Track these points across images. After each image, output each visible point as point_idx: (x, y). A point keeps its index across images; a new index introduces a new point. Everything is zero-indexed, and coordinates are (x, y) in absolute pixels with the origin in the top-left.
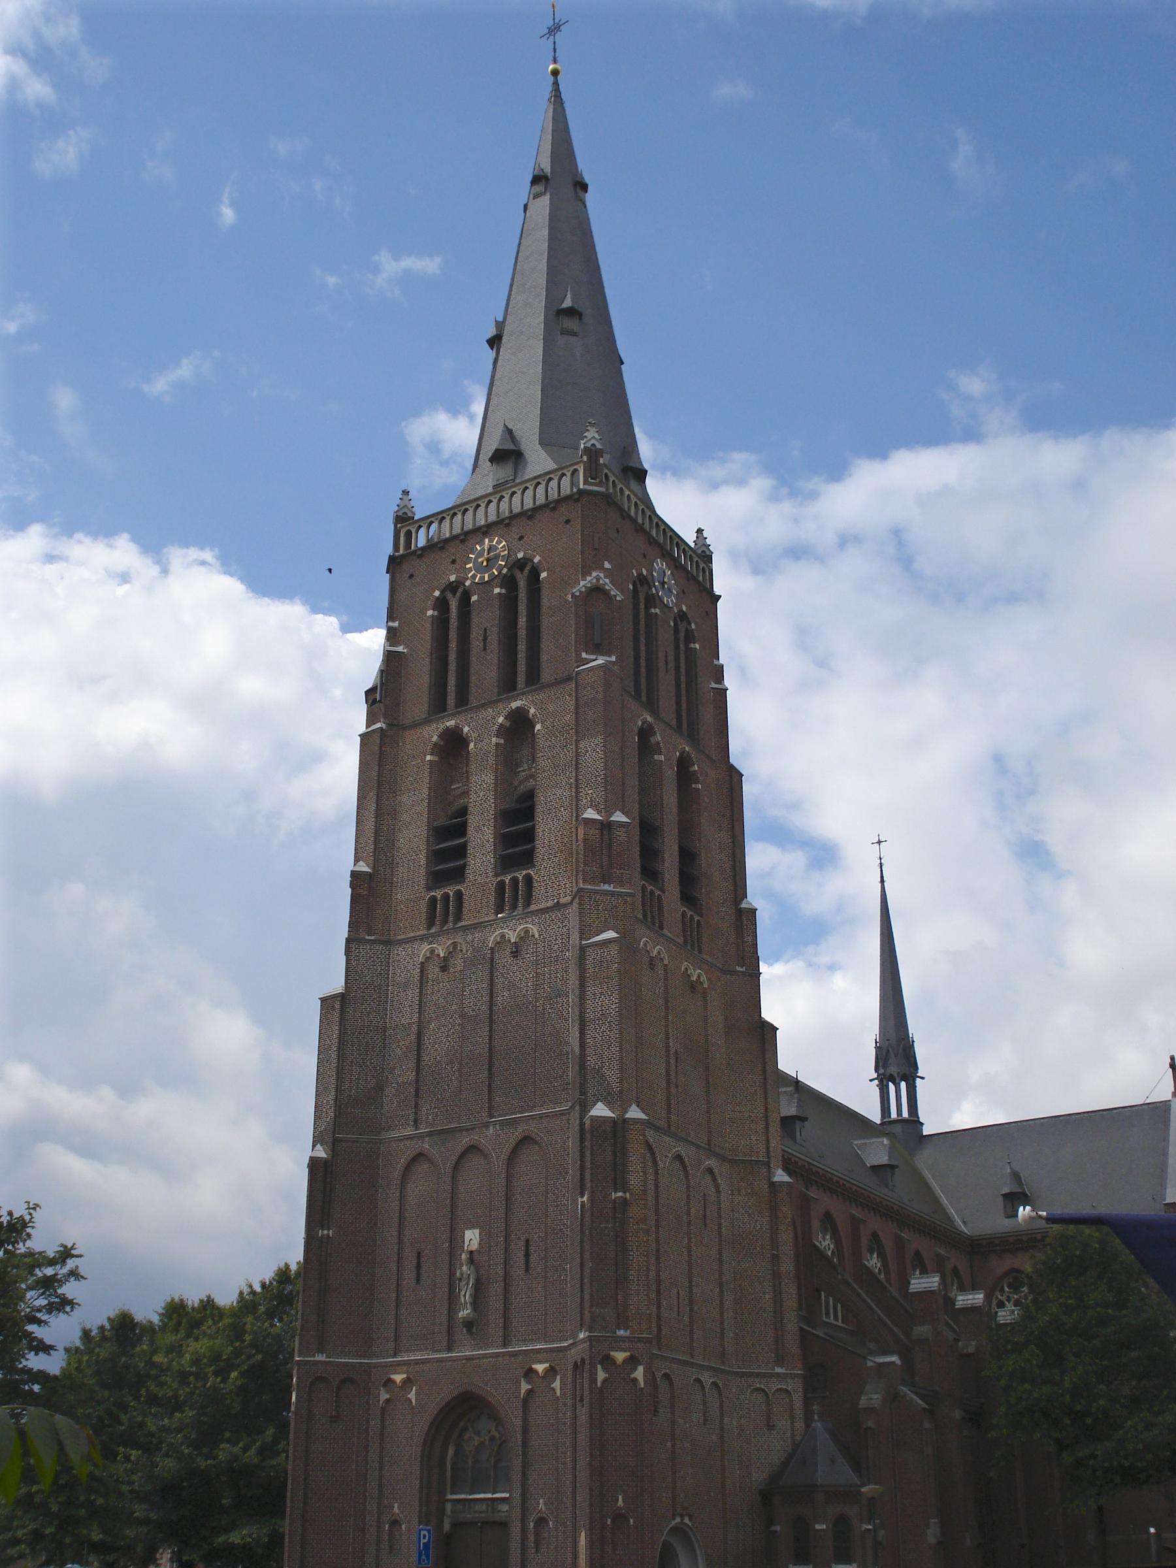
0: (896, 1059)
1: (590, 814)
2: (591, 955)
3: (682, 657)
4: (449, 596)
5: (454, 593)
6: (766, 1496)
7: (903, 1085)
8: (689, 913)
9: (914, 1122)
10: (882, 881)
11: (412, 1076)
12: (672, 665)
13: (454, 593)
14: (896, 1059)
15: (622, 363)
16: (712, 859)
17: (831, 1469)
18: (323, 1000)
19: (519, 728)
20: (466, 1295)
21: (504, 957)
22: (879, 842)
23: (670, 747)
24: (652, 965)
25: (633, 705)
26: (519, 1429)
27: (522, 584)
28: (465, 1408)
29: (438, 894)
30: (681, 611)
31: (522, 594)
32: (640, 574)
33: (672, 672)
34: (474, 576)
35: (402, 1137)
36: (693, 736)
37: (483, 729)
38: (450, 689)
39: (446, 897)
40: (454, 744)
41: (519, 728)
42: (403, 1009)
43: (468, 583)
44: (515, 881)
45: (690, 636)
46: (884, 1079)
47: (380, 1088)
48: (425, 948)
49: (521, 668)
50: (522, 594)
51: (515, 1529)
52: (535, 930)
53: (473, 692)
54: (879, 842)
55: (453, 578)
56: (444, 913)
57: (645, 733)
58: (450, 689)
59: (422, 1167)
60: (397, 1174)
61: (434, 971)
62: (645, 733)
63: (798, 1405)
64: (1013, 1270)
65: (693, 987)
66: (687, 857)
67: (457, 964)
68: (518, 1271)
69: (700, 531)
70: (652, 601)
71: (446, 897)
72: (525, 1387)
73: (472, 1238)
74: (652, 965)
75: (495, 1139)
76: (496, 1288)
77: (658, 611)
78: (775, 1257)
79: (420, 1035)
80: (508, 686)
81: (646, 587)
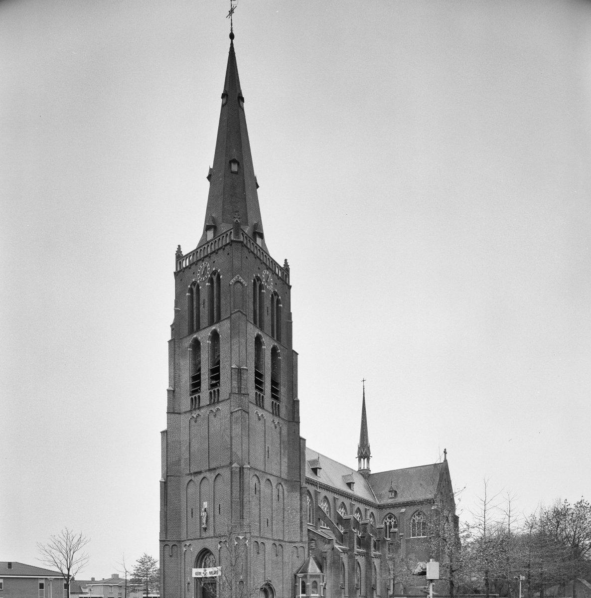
0: (364, 453)
3: (275, 309)
4: (193, 287)
5: (195, 286)
7: (366, 459)
8: (275, 402)
9: (368, 470)
10: (364, 394)
11: (188, 456)
12: (270, 312)
13: (195, 286)
14: (364, 453)
15: (258, 187)
17: (313, 568)
18: (161, 432)
19: (215, 336)
20: (204, 521)
22: (364, 381)
23: (268, 344)
26: (218, 558)
29: (193, 397)
30: (274, 292)
31: (215, 285)
32: (257, 276)
33: (270, 315)
34: (200, 279)
36: (279, 340)
37: (204, 336)
39: (195, 397)
41: (215, 336)
43: (198, 282)
44: (214, 391)
45: (278, 302)
47: (180, 460)
50: (215, 285)
54: (364, 381)
55: (194, 280)
58: (194, 327)
59: (192, 483)
60: (185, 486)
61: (193, 423)
64: (390, 513)
69: (286, 260)
70: (261, 287)
71: (195, 397)
73: (205, 505)
76: (211, 519)
77: (265, 291)
79: (190, 443)
81: (260, 282)
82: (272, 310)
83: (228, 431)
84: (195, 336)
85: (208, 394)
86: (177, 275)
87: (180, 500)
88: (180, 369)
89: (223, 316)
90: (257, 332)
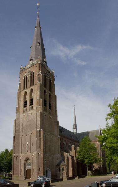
0: (75, 127)
1: (38, 99)
2: (38, 114)
6: (57, 166)
14: (75, 127)
16: (53, 105)
19: (32, 90)
20: (27, 148)
21: (30, 115)
23: (48, 92)
24: (45, 115)
25: (43, 87)
27: (32, 74)
28: (27, 159)
35: (21, 134)
37: (28, 91)
38: (25, 87)
40: (26, 93)
41: (32, 90)
42: (21, 121)
46: (74, 128)
47: (19, 129)
48: (23, 114)
49: (32, 83)
51: (32, 170)
52: (33, 112)
53: (27, 87)
56: (25, 111)
57: (45, 91)
58: (25, 87)
62: (45, 91)
63: (60, 157)
65: (50, 118)
66: (50, 104)
67: (26, 116)
68: (31, 146)
72: (32, 156)
73: (28, 143)
74: (45, 115)
75: (29, 133)
78: (58, 144)
80: (31, 86)
82: (49, 83)
83: (36, 119)
84: (25, 90)
85: (29, 108)
86: (60, 130)
87: (19, 142)
88: (20, 101)
89: (35, 83)
90: (45, 89)
